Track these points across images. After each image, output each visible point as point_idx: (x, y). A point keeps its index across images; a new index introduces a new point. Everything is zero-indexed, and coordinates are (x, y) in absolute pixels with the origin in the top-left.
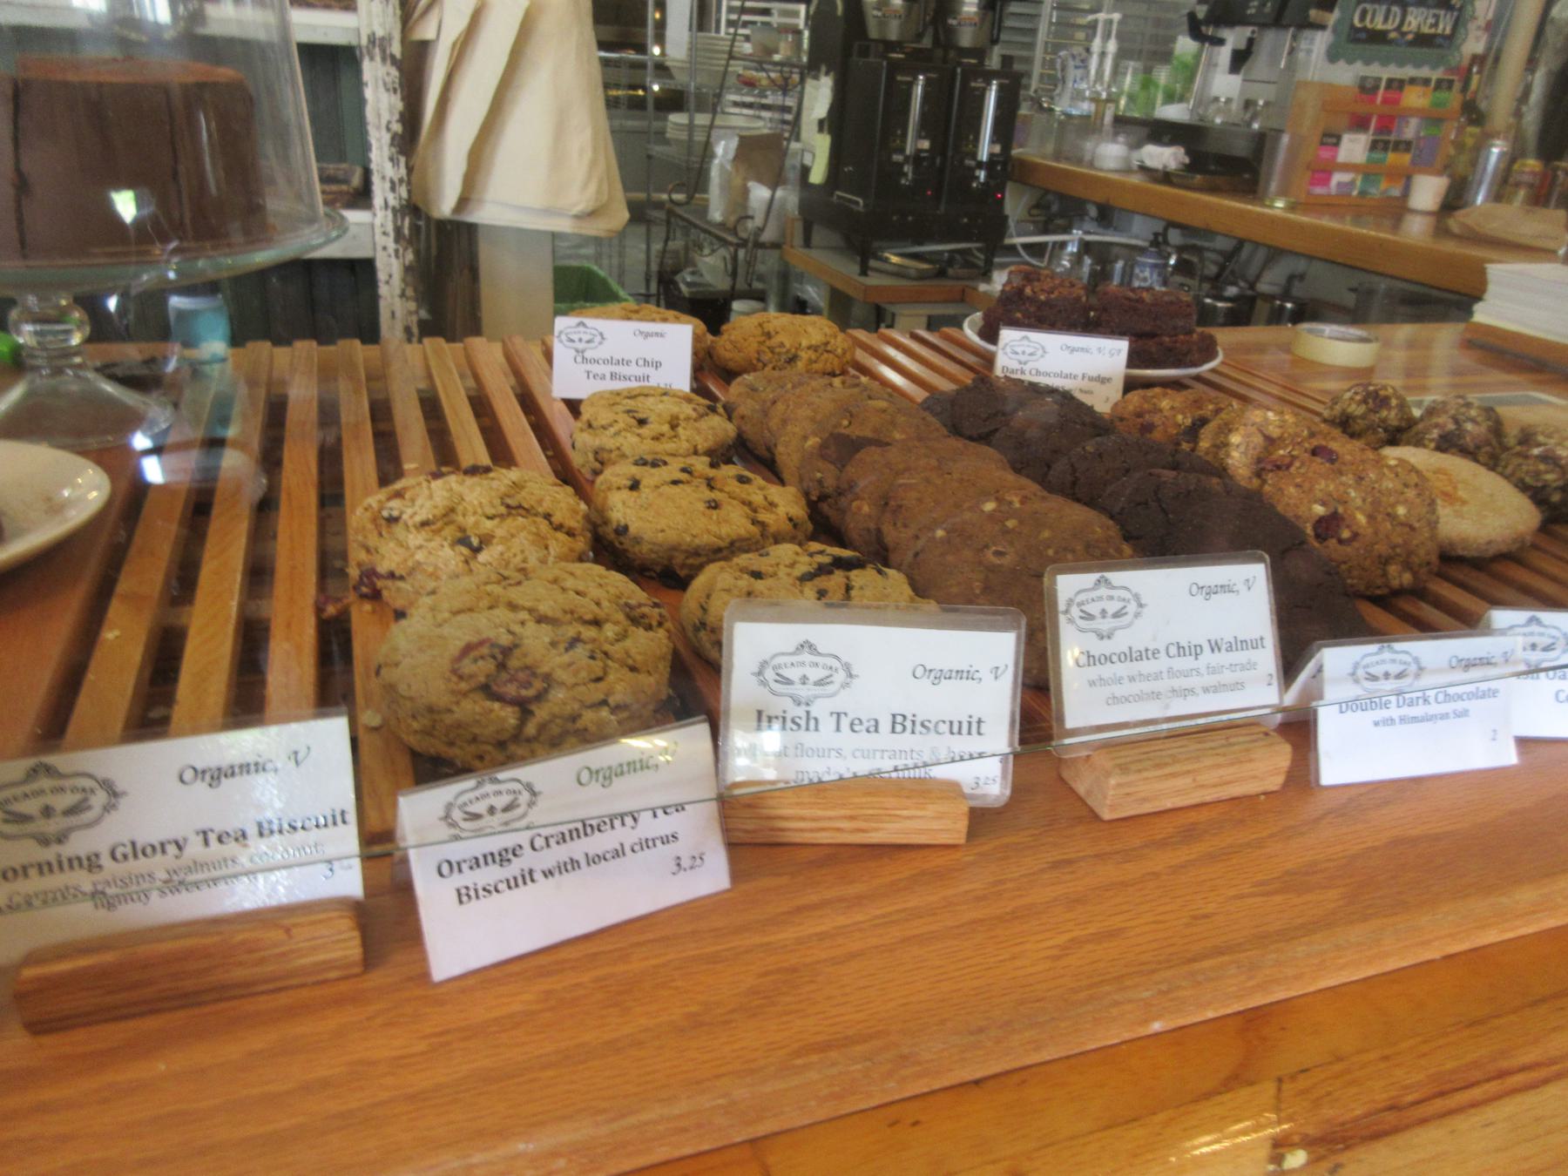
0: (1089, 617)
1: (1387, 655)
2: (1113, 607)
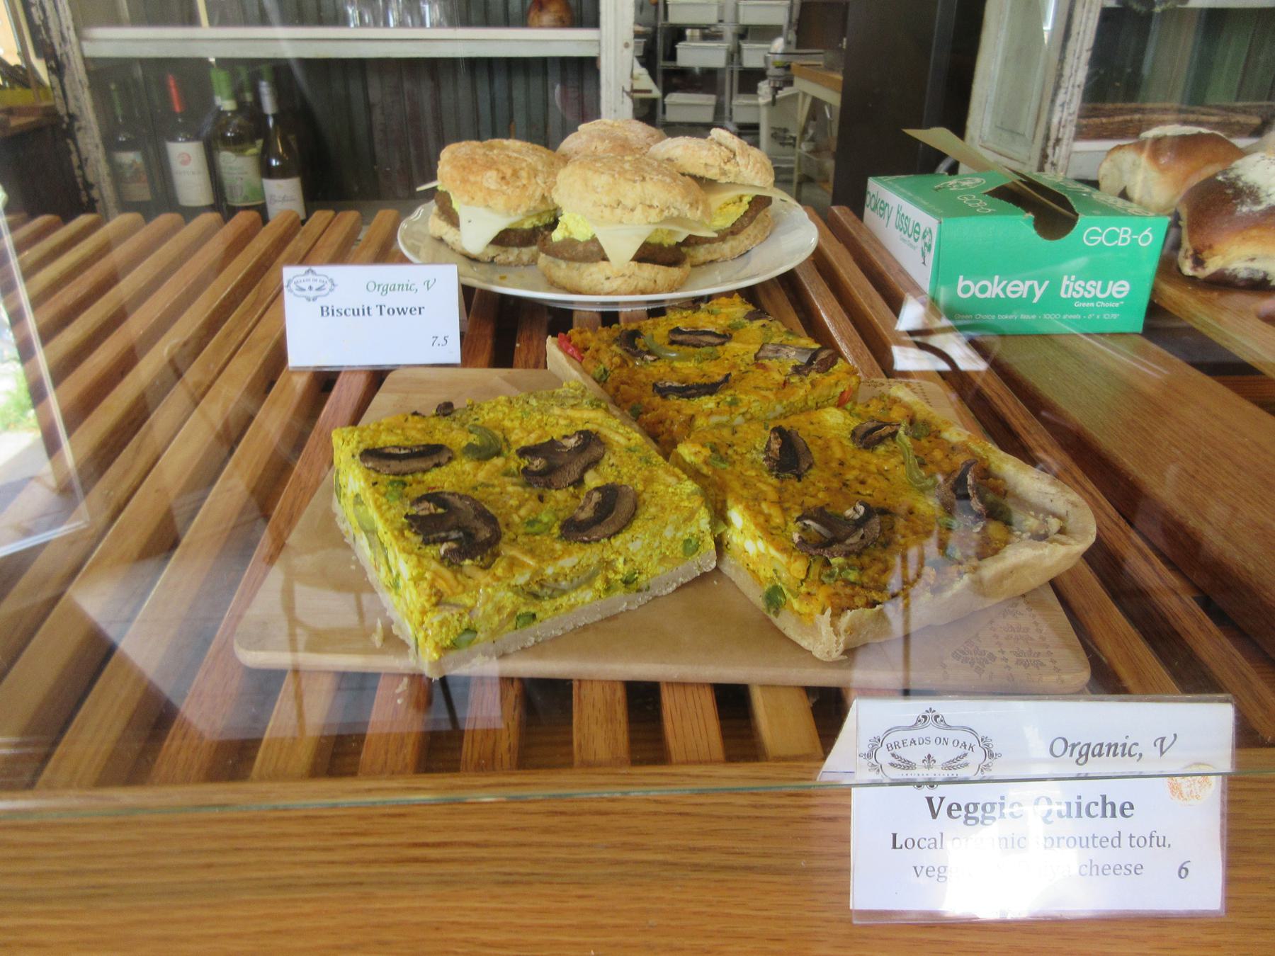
0: (303, 290)
1: (310, 276)
2: (316, 285)
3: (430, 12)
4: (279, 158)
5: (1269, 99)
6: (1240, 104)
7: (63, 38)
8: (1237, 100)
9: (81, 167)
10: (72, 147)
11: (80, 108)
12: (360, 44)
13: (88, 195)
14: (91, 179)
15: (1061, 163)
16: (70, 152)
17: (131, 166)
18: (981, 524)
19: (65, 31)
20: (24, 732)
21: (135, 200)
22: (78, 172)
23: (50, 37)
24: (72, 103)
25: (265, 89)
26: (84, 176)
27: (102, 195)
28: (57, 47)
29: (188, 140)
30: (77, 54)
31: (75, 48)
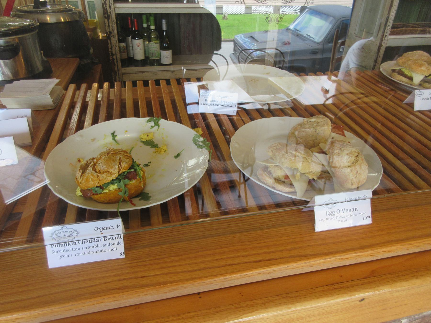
3: (185, 2)
4: (166, 43)
5: (424, 21)
6: (418, 23)
7: (110, 8)
8: (417, 22)
9: (111, 48)
10: (109, 42)
11: (113, 29)
12: (182, 9)
13: (113, 57)
14: (114, 52)
15: (386, 42)
16: (109, 44)
17: (123, 47)
18: (43, 90)
19: (111, 5)
20: (28, 235)
21: (137, 59)
22: (110, 50)
23: (106, 7)
24: (111, 28)
25: (164, 22)
26: (112, 52)
27: (116, 57)
28: (108, 10)
29: (140, 39)
30: (114, 12)
31: (113, 11)
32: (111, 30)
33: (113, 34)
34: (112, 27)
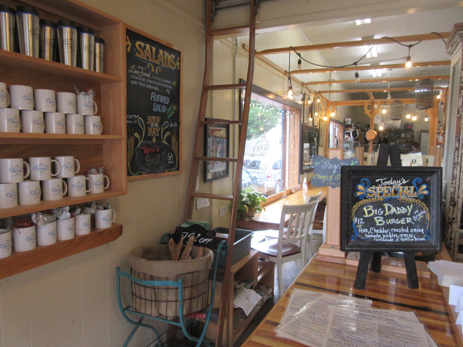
7: (458, 197)
32: (454, 216)
33: (456, 221)
34: (457, 214)
